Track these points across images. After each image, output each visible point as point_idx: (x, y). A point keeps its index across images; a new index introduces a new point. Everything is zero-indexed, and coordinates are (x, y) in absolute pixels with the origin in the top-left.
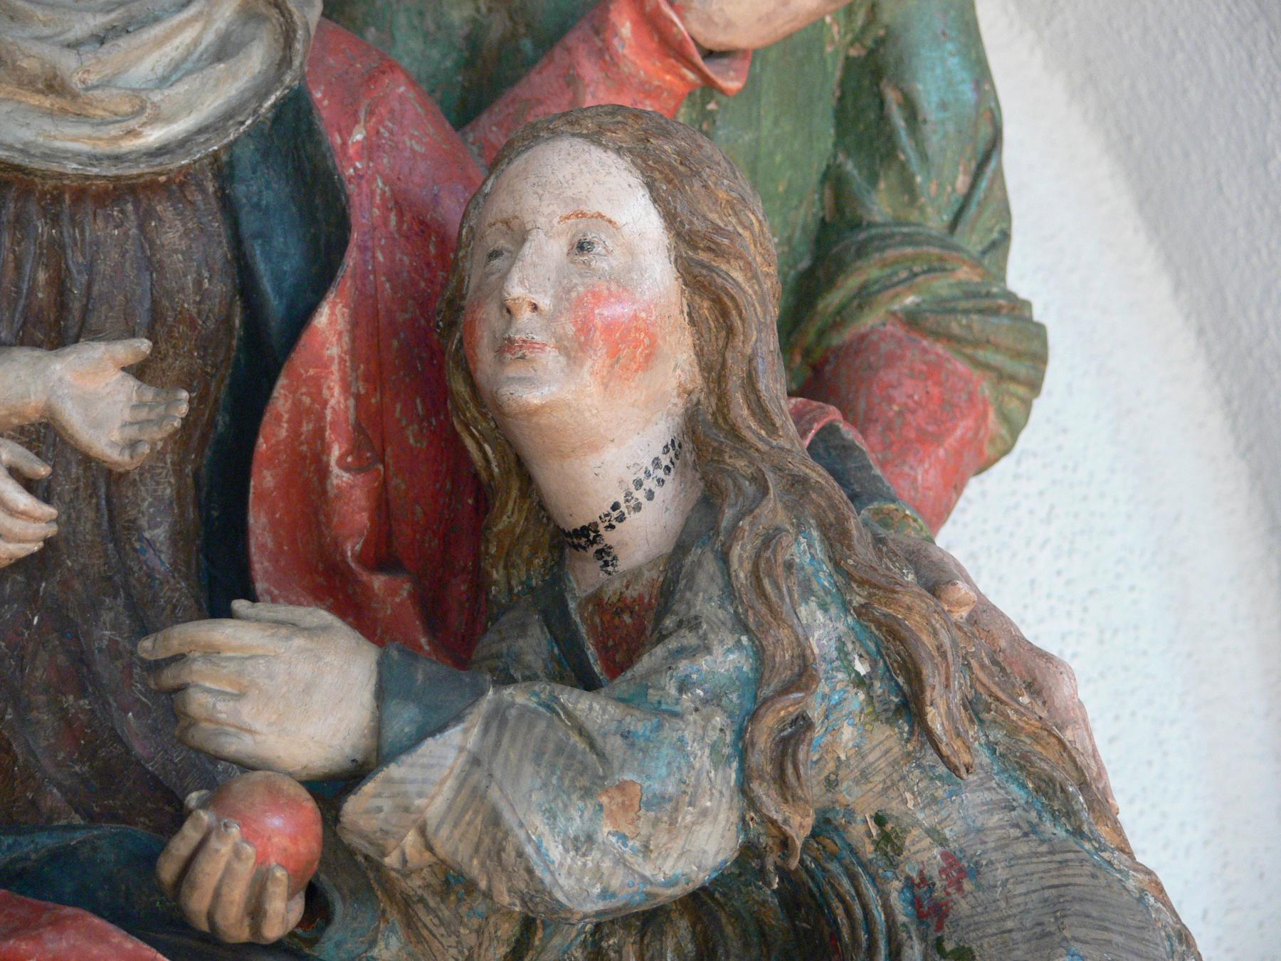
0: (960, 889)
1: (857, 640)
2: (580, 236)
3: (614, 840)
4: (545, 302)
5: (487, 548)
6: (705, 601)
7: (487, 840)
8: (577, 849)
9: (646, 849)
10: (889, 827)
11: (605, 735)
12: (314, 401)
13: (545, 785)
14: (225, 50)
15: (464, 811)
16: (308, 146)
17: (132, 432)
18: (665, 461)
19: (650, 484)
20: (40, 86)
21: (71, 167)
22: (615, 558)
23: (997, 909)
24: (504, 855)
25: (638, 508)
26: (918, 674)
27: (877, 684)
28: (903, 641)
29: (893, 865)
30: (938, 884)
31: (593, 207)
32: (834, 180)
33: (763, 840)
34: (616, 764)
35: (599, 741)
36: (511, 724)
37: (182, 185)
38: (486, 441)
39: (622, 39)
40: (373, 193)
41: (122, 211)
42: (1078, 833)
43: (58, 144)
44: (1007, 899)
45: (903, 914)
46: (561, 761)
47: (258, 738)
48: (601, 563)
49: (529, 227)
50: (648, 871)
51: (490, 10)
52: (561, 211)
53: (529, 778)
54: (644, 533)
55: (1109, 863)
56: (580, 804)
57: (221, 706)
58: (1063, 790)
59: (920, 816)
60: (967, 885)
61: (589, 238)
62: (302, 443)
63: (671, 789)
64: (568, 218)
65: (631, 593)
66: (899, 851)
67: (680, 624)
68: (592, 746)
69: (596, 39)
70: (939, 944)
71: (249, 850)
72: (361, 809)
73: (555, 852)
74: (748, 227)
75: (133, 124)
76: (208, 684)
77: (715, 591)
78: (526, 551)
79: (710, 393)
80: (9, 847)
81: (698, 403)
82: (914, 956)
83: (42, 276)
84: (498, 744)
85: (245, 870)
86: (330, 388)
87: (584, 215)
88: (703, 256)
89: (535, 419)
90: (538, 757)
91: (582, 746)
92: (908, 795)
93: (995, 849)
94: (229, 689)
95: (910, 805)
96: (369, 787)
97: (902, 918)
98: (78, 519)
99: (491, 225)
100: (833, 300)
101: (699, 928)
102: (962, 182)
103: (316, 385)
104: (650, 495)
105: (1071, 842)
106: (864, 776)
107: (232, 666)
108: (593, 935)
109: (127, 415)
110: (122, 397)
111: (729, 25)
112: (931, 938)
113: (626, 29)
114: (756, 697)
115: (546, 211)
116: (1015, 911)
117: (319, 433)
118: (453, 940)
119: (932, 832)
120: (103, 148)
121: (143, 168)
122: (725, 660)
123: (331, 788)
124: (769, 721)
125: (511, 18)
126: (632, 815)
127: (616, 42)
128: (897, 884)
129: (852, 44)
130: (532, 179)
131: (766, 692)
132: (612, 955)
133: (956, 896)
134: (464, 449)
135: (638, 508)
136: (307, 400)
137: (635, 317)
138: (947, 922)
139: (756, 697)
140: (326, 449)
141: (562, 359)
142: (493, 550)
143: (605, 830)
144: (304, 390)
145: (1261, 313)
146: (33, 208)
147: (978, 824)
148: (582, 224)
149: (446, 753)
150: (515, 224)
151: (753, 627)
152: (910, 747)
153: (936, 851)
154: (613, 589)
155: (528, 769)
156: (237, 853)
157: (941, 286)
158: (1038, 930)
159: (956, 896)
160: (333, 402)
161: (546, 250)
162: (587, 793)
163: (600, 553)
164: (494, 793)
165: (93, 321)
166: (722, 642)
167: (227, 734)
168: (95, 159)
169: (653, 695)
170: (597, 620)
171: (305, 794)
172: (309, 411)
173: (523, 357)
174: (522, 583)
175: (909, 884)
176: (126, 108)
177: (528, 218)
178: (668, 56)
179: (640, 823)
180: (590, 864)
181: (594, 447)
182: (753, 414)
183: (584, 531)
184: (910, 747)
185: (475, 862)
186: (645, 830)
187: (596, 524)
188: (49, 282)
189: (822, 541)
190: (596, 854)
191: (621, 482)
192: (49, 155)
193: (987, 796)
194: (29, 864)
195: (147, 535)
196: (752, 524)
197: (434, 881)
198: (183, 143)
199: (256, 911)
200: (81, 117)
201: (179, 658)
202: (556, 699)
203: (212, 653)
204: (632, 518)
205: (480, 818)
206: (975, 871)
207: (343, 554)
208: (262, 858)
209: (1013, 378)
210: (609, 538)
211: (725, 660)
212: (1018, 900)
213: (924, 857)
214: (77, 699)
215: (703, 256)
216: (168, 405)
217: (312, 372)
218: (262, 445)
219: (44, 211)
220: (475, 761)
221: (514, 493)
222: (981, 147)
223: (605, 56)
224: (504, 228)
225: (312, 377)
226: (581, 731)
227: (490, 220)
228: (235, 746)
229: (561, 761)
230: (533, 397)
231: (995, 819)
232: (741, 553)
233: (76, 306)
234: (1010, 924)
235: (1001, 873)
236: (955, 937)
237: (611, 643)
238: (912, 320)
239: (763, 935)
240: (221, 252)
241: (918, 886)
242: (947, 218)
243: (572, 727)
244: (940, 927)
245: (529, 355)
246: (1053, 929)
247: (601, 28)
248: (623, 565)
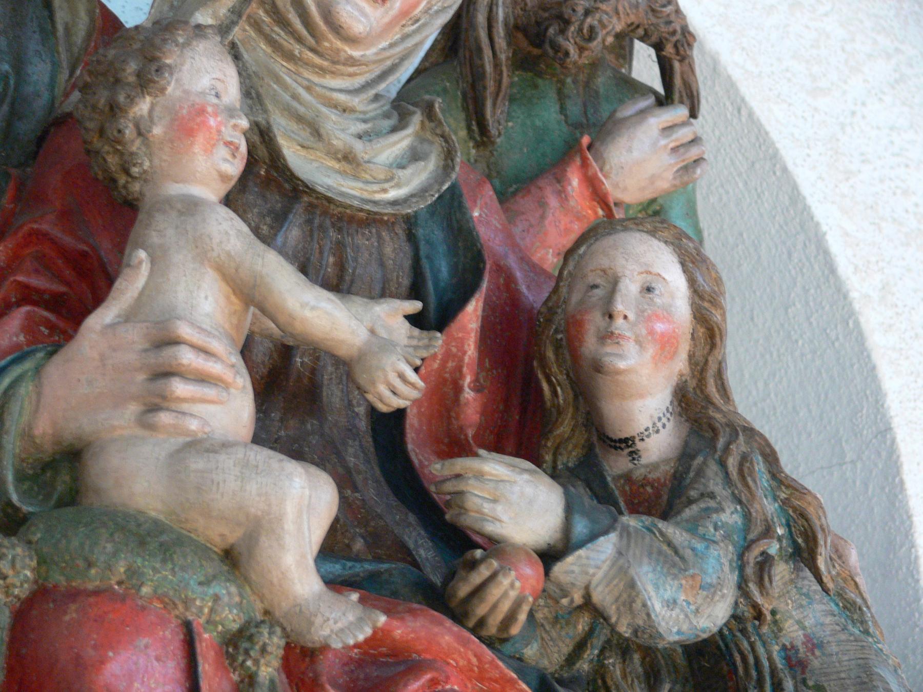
0: (813, 654)
1: (778, 517)
2: (648, 284)
3: (685, 603)
4: (631, 316)
5: (546, 443)
6: (714, 482)
7: (625, 596)
8: (668, 606)
9: (697, 611)
10: (778, 617)
11: (684, 548)
12: (458, 350)
13: (654, 570)
15: (614, 578)
16: (458, 215)
19: (664, 420)
20: (340, 156)
21: (356, 203)
22: (640, 457)
23: (835, 667)
24: (634, 605)
25: (658, 431)
26: (815, 540)
27: (784, 541)
28: (807, 520)
29: (777, 637)
30: (801, 650)
31: (655, 270)
33: (746, 614)
34: (691, 564)
35: (681, 551)
36: (633, 535)
37: (393, 223)
38: (559, 385)
39: (573, 187)
41: (370, 232)
42: (866, 632)
43: (343, 189)
44: (839, 662)
45: (780, 664)
46: (662, 559)
47: (504, 525)
48: (630, 458)
49: (620, 275)
51: (476, 161)
52: (638, 269)
55: (881, 650)
56: (671, 582)
57: (486, 505)
58: (860, 609)
59: (794, 613)
60: (817, 653)
61: (653, 285)
62: (446, 372)
63: (715, 581)
64: (642, 273)
65: (652, 476)
66: (780, 630)
67: (702, 495)
68: (676, 552)
69: (558, 185)
70: (804, 682)
71: (518, 584)
75: (386, 186)
76: (476, 492)
77: (719, 480)
78: (570, 447)
79: (693, 376)
80: (350, 568)
81: (686, 381)
82: (789, 684)
83: (331, 260)
84: (628, 545)
85: (513, 594)
86: (469, 345)
87: (651, 273)
88: (706, 304)
89: (621, 378)
90: (650, 554)
91: (670, 552)
92: (789, 601)
93: (830, 635)
94: (487, 496)
95: (790, 607)
96: (570, 559)
97: (780, 666)
98: (332, 395)
99: (592, 271)
101: (648, 659)
104: (664, 426)
105: (863, 637)
107: (492, 485)
108: (598, 656)
110: (403, 331)
111: (625, 189)
112: (799, 677)
114: (745, 538)
115: (630, 267)
116: (844, 668)
117: (459, 369)
118: (556, 649)
119: (799, 622)
120: (366, 195)
121: (389, 210)
123: (549, 556)
125: (488, 167)
126: (695, 592)
127: (569, 188)
128: (777, 648)
129: (640, 211)
130: (621, 250)
131: (751, 536)
132: (611, 668)
133: (811, 657)
134: (541, 390)
135: (658, 431)
136: (454, 350)
137: (674, 331)
138: (807, 671)
139: (745, 538)
140: (462, 377)
141: (637, 347)
142: (549, 444)
144: (453, 344)
145: (766, 384)
146: (328, 222)
147: (821, 621)
148: (649, 278)
149: (607, 545)
150: (609, 272)
151: (745, 501)
152: (793, 576)
153: (801, 633)
154: (638, 474)
155: (646, 560)
156: (512, 586)
158: (858, 680)
159: (811, 657)
160: (470, 353)
161: (630, 287)
163: (631, 453)
164: (632, 572)
165: (353, 289)
166: (729, 507)
167: (488, 521)
169: (701, 530)
170: (627, 488)
171: (535, 556)
172: (455, 356)
173: (618, 343)
174: (563, 464)
175: (784, 648)
176: (382, 176)
177: (619, 270)
178: (594, 200)
179: (698, 597)
180: (674, 615)
181: (642, 396)
182: (718, 391)
183: (626, 440)
184: (793, 576)
185: (614, 607)
186: (699, 601)
187: (634, 437)
188: (335, 264)
189: (764, 462)
190: (677, 610)
191: (651, 417)
192: (343, 194)
193: (824, 607)
194: (358, 579)
195: (356, 410)
196: (737, 448)
197: (549, 616)
200: (356, 178)
201: (458, 476)
202: (656, 526)
203: (480, 476)
205: (623, 583)
206: (821, 645)
207: (466, 435)
208: (523, 588)
210: (639, 445)
212: (845, 663)
213: (794, 635)
214: (352, 492)
215: (706, 304)
216: (430, 339)
217: (460, 335)
219: (333, 225)
221: (570, 415)
223: (562, 194)
224: (601, 273)
225: (459, 338)
226: (670, 544)
227: (591, 267)
228: (490, 528)
229: (662, 559)
230: (622, 365)
232: (732, 463)
233: (347, 278)
234: (843, 675)
236: (813, 678)
237: (636, 501)
239: (675, 666)
240: (407, 263)
241: (790, 650)
243: (663, 542)
244: (803, 673)
245: (622, 343)
246: (867, 680)
247: (560, 179)
248: (644, 461)
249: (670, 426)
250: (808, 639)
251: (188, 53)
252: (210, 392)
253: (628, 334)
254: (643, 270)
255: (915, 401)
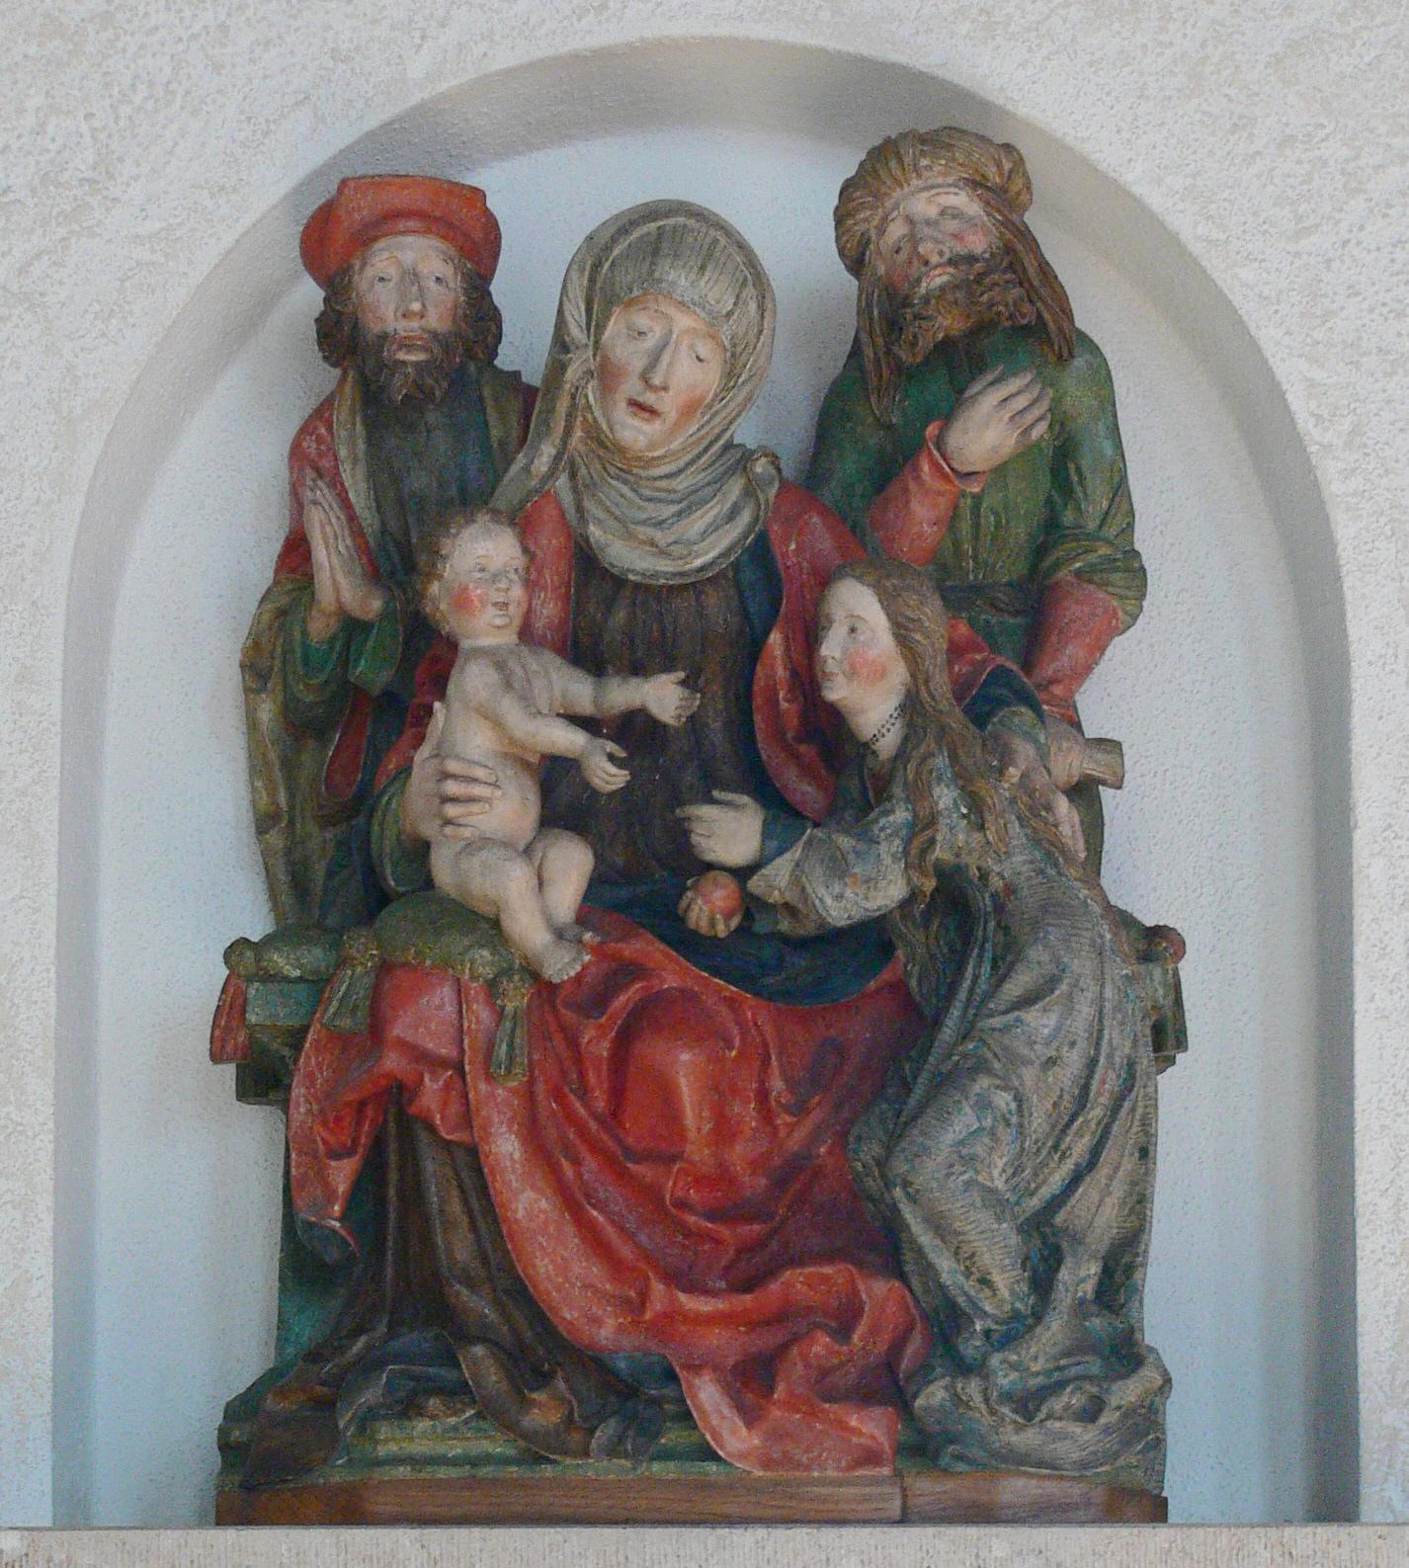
9: (867, 898)
14: (732, 515)
17: (679, 711)
18: (895, 715)
25: (883, 736)
27: (973, 817)
29: (986, 886)
32: (1049, 501)
40: (801, 569)
50: (868, 905)
53: (819, 871)
54: (888, 744)
60: (1012, 898)
72: (755, 884)
73: (829, 901)
74: (926, 615)
88: (903, 632)
100: (1047, 563)
102: (1105, 504)
103: (772, 667)
104: (889, 730)
106: (970, 853)
109: (678, 703)
113: (926, 468)
122: (901, 815)
123: (742, 874)
124: (916, 843)
143: (848, 893)
156: (701, 909)
157: (1092, 558)
162: (841, 878)
168: (674, 575)
175: (992, 895)
190: (844, 901)
198: (712, 563)
199: (712, 923)
204: (881, 740)
209: (1127, 598)
211: (901, 815)
218: (755, 688)
220: (797, 865)
222: (1115, 485)
223: (918, 479)
231: (1025, 868)
235: (1025, 892)
238: (1078, 573)
240: (735, 603)
242: (1098, 522)
247: (917, 468)
248: (881, 758)
249: (898, 725)
250: (1006, 886)
251: (458, 542)
252: (475, 808)
253: (835, 671)
254: (461, 829)
255: (1373, 541)
